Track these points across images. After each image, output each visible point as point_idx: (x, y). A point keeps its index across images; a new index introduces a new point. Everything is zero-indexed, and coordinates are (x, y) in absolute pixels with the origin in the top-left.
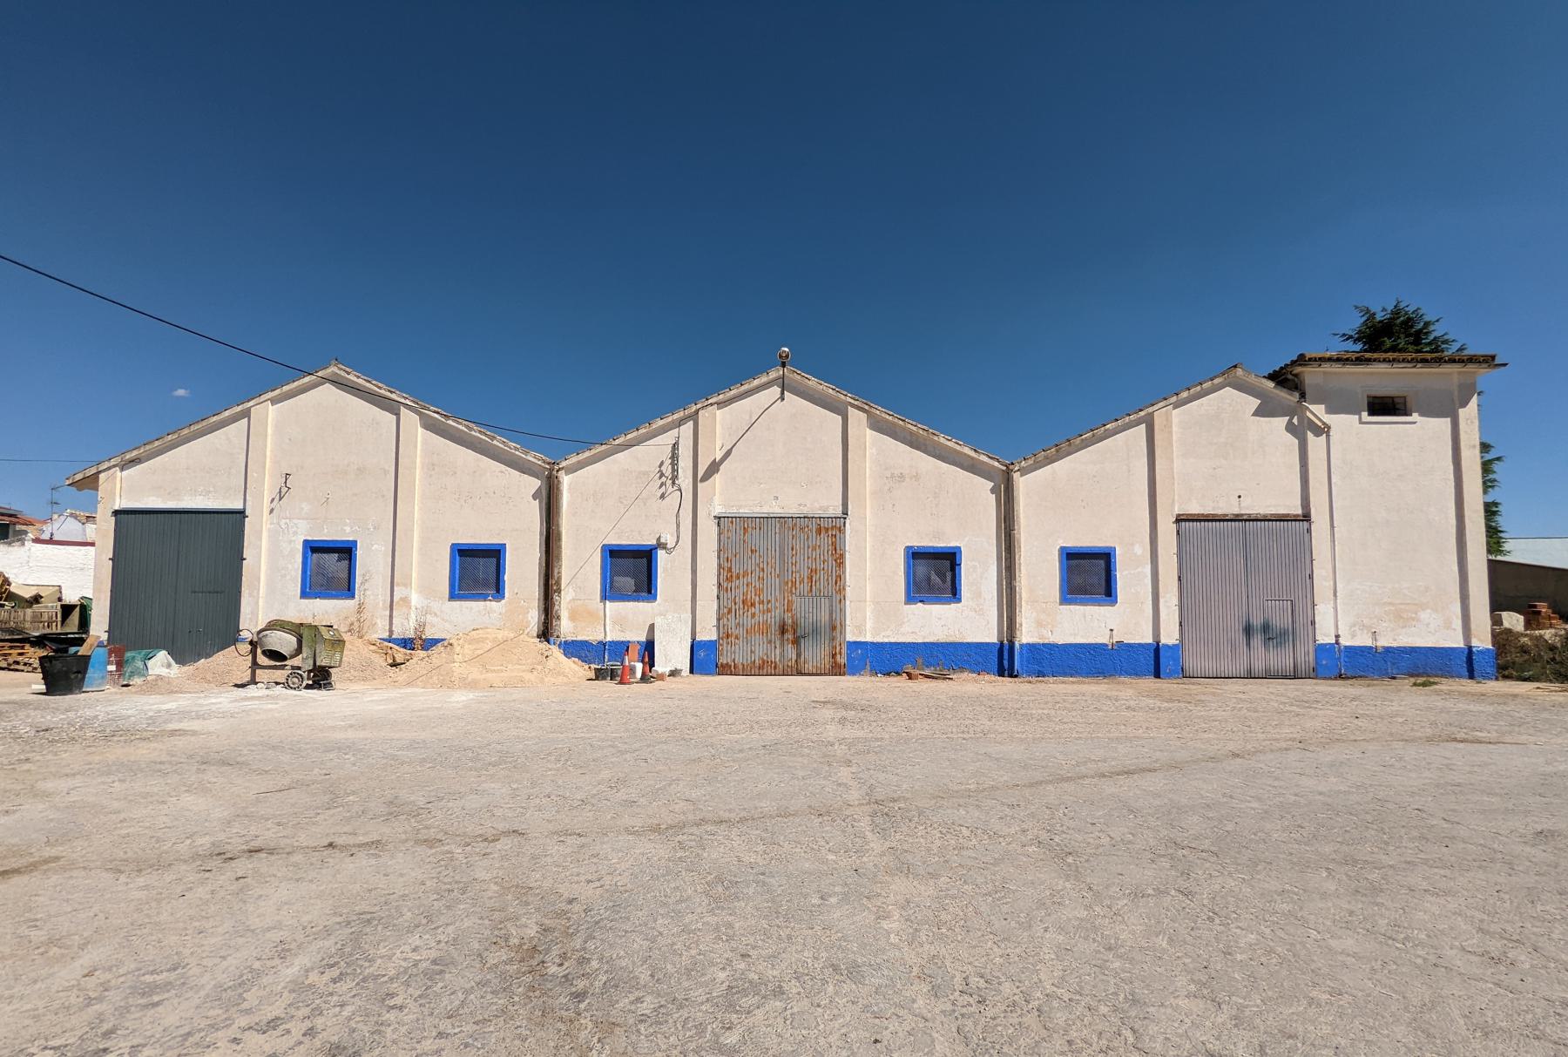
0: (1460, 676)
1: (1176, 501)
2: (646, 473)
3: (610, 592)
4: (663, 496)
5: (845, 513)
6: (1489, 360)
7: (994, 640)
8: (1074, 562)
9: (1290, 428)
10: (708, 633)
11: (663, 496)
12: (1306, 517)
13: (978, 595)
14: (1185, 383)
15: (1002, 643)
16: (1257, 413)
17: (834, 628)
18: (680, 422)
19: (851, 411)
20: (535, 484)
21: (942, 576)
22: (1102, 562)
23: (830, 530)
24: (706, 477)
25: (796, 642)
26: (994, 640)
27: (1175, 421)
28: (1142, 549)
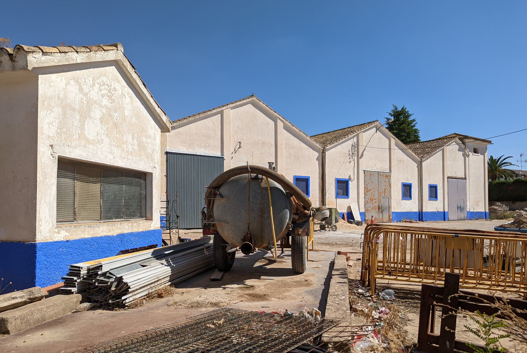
0: (483, 219)
1: (448, 173)
2: (345, 153)
3: (338, 196)
4: (350, 162)
5: (390, 171)
6: (490, 142)
7: (417, 211)
8: (340, 184)
9: (463, 155)
10: (362, 210)
11: (350, 162)
12: (465, 179)
13: (415, 197)
14: (234, 99)
15: (419, 212)
16: (492, 157)
17: (389, 207)
18: (354, 137)
19: (279, 121)
20: (316, 154)
21: (407, 192)
22: (305, 183)
23: (388, 176)
24: (361, 157)
25: (382, 212)
26: (417, 211)
27: (364, 136)
28: (441, 186)
